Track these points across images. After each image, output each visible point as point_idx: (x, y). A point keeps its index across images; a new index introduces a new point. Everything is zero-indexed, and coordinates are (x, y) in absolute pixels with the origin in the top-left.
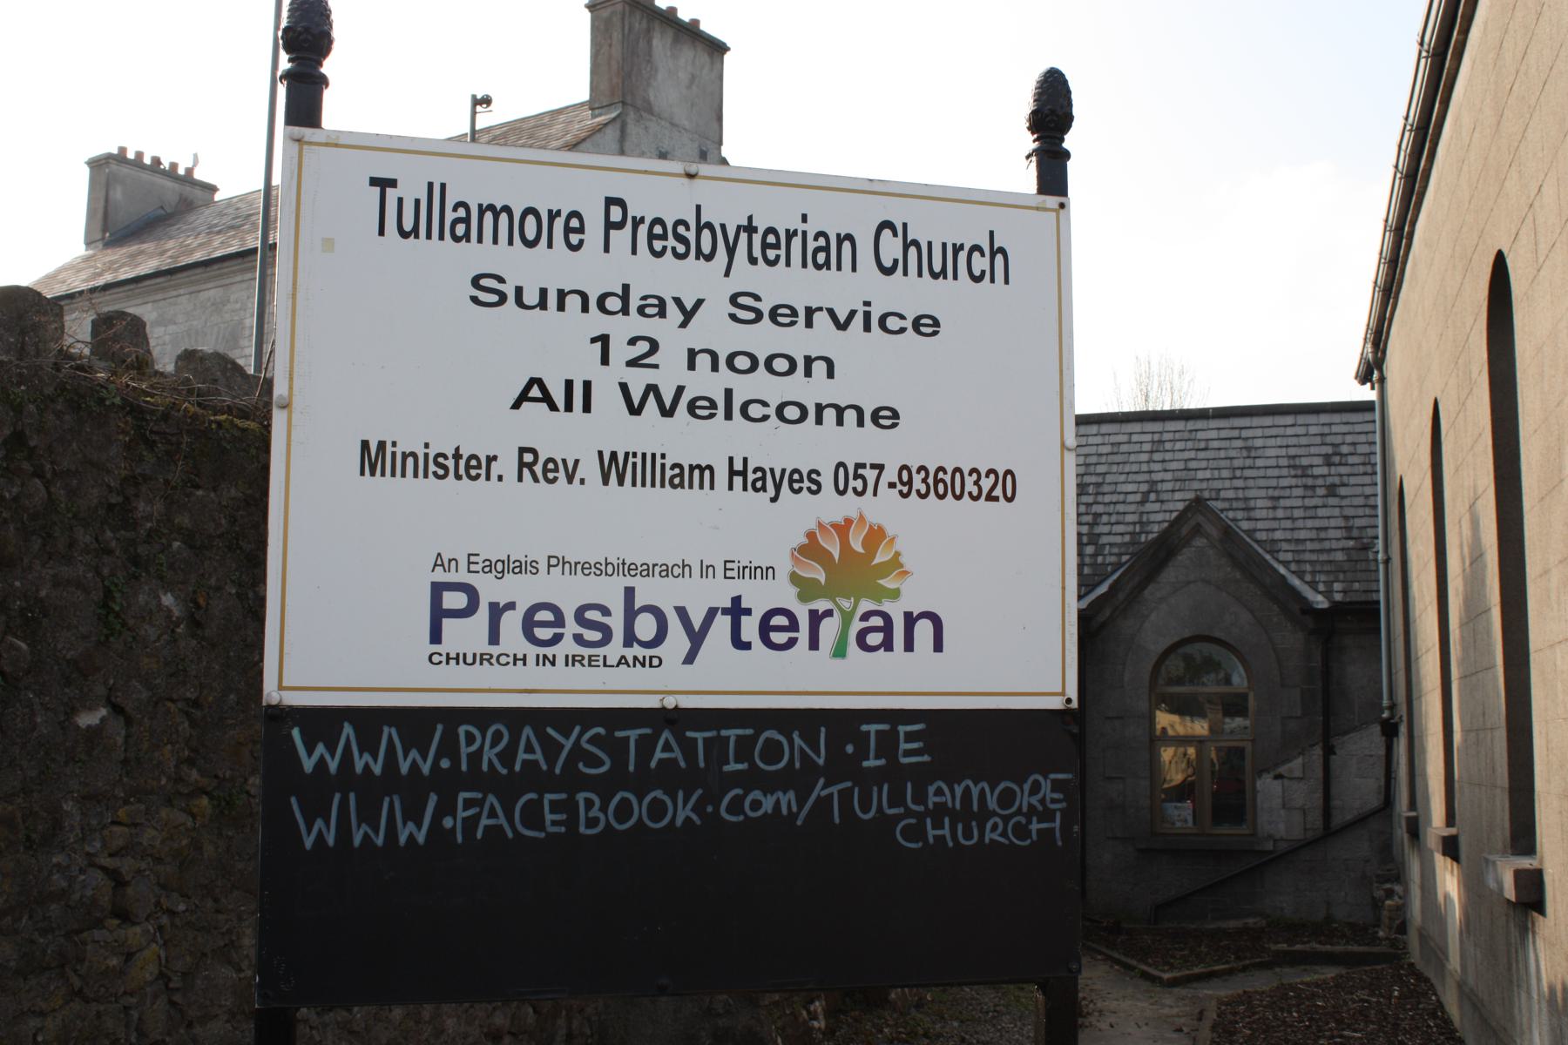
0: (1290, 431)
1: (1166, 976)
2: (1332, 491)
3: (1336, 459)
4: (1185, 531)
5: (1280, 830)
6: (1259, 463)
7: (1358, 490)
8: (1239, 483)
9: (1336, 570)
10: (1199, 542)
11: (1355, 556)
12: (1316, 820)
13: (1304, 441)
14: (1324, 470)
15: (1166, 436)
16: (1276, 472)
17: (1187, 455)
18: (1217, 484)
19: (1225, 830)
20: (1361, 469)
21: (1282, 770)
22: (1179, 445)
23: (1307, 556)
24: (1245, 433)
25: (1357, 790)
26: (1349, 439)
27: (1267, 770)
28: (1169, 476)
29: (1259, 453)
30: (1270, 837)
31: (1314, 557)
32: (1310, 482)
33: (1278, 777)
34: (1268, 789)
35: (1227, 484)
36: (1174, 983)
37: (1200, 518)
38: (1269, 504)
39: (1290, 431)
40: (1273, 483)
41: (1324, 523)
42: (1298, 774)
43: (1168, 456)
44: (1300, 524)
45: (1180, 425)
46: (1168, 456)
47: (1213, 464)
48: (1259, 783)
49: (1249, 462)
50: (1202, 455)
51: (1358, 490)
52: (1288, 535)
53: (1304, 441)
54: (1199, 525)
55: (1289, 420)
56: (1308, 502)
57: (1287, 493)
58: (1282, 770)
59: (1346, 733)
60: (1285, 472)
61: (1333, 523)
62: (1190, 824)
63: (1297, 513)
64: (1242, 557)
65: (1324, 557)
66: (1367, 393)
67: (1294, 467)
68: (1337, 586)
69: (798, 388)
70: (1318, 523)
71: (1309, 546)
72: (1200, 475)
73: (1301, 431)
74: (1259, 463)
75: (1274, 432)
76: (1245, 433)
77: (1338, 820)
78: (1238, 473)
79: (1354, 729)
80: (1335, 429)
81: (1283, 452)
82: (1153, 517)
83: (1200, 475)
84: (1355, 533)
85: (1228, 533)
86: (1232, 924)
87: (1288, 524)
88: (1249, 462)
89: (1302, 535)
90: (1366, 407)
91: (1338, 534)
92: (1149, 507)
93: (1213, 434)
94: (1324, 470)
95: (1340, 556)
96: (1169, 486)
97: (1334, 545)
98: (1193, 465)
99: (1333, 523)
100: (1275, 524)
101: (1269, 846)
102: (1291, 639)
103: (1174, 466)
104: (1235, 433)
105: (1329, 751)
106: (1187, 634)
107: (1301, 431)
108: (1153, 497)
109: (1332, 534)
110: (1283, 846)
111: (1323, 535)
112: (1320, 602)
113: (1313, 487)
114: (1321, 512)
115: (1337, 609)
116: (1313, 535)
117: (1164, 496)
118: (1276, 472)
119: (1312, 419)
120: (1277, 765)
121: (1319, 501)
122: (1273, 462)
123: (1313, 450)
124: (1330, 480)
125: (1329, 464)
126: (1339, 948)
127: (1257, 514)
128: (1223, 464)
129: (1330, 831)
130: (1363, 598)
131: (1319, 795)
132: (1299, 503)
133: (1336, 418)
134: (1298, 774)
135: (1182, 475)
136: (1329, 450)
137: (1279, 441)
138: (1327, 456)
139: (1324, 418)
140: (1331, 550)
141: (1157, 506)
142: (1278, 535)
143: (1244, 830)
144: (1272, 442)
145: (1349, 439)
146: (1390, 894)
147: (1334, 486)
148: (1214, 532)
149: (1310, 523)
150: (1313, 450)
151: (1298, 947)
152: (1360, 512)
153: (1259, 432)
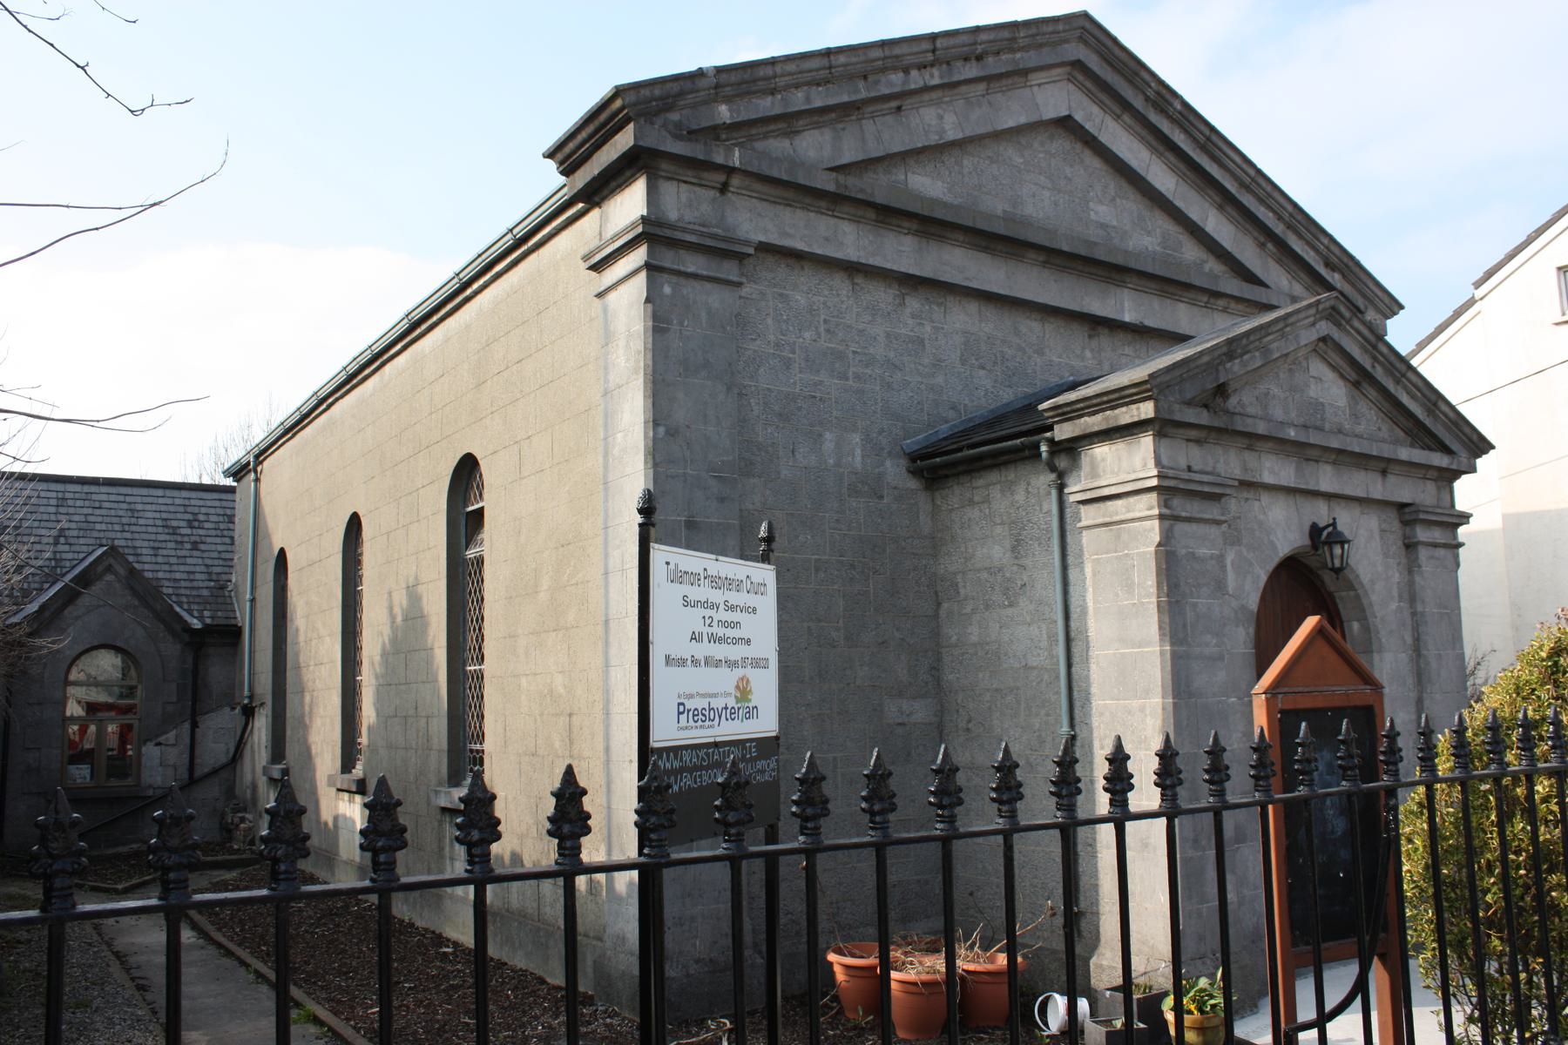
0: (161, 501)
1: (120, 887)
4: (100, 569)
6: (141, 522)
7: (213, 547)
8: (128, 535)
9: (205, 602)
10: (109, 577)
11: (215, 592)
12: (183, 773)
13: (172, 509)
14: (188, 531)
15: (68, 495)
16: (154, 530)
17: (85, 511)
18: (112, 535)
19: (114, 782)
20: (213, 533)
22: (79, 503)
23: (183, 591)
24: (128, 499)
25: (214, 750)
26: (203, 510)
28: (73, 525)
30: (150, 786)
33: (159, 744)
34: (151, 752)
35: (119, 535)
37: (112, 561)
39: (161, 501)
40: (153, 537)
41: (192, 569)
42: (172, 741)
43: (71, 510)
45: (78, 488)
46: (71, 510)
47: (108, 520)
48: (144, 749)
49: (133, 520)
50: (98, 512)
51: (213, 547)
52: (168, 575)
53: (172, 509)
55: (160, 492)
58: (161, 739)
60: (160, 530)
61: (198, 569)
63: (173, 560)
64: (143, 591)
65: (195, 593)
68: (206, 613)
69: (730, 633)
70: (187, 568)
71: (183, 584)
72: (98, 527)
74: (141, 522)
75: (150, 500)
76: (128, 499)
79: (212, 710)
80: (193, 502)
82: (64, 556)
83: (98, 527)
85: (133, 572)
87: (167, 567)
88: (133, 520)
89: (178, 576)
91: (203, 577)
92: (60, 548)
93: (104, 497)
94: (188, 531)
95: (205, 593)
96: (75, 533)
98: (91, 519)
99: (198, 569)
100: (157, 567)
101: (150, 793)
102: (172, 649)
103: (76, 518)
104: (121, 498)
105: (194, 726)
106: (96, 643)
107: (169, 501)
108: (62, 540)
109: (198, 576)
110: (159, 792)
112: (196, 624)
114: (189, 561)
115: (208, 630)
116: (185, 576)
117: (72, 541)
118: (154, 530)
119: (176, 493)
121: (187, 553)
122: (151, 522)
123: (179, 516)
124: (193, 539)
125: (192, 527)
126: (220, 858)
127: (145, 559)
128: (115, 520)
129: (193, 780)
131: (186, 756)
132: (173, 553)
133: (193, 494)
134: (172, 741)
135: (84, 525)
136: (190, 517)
137: (154, 507)
139: (185, 494)
141: (66, 548)
142: (160, 575)
143: (130, 781)
144: (149, 507)
145: (203, 510)
146: (243, 820)
147: (195, 543)
148: (122, 571)
149: (182, 568)
150: (179, 516)
153: (139, 499)
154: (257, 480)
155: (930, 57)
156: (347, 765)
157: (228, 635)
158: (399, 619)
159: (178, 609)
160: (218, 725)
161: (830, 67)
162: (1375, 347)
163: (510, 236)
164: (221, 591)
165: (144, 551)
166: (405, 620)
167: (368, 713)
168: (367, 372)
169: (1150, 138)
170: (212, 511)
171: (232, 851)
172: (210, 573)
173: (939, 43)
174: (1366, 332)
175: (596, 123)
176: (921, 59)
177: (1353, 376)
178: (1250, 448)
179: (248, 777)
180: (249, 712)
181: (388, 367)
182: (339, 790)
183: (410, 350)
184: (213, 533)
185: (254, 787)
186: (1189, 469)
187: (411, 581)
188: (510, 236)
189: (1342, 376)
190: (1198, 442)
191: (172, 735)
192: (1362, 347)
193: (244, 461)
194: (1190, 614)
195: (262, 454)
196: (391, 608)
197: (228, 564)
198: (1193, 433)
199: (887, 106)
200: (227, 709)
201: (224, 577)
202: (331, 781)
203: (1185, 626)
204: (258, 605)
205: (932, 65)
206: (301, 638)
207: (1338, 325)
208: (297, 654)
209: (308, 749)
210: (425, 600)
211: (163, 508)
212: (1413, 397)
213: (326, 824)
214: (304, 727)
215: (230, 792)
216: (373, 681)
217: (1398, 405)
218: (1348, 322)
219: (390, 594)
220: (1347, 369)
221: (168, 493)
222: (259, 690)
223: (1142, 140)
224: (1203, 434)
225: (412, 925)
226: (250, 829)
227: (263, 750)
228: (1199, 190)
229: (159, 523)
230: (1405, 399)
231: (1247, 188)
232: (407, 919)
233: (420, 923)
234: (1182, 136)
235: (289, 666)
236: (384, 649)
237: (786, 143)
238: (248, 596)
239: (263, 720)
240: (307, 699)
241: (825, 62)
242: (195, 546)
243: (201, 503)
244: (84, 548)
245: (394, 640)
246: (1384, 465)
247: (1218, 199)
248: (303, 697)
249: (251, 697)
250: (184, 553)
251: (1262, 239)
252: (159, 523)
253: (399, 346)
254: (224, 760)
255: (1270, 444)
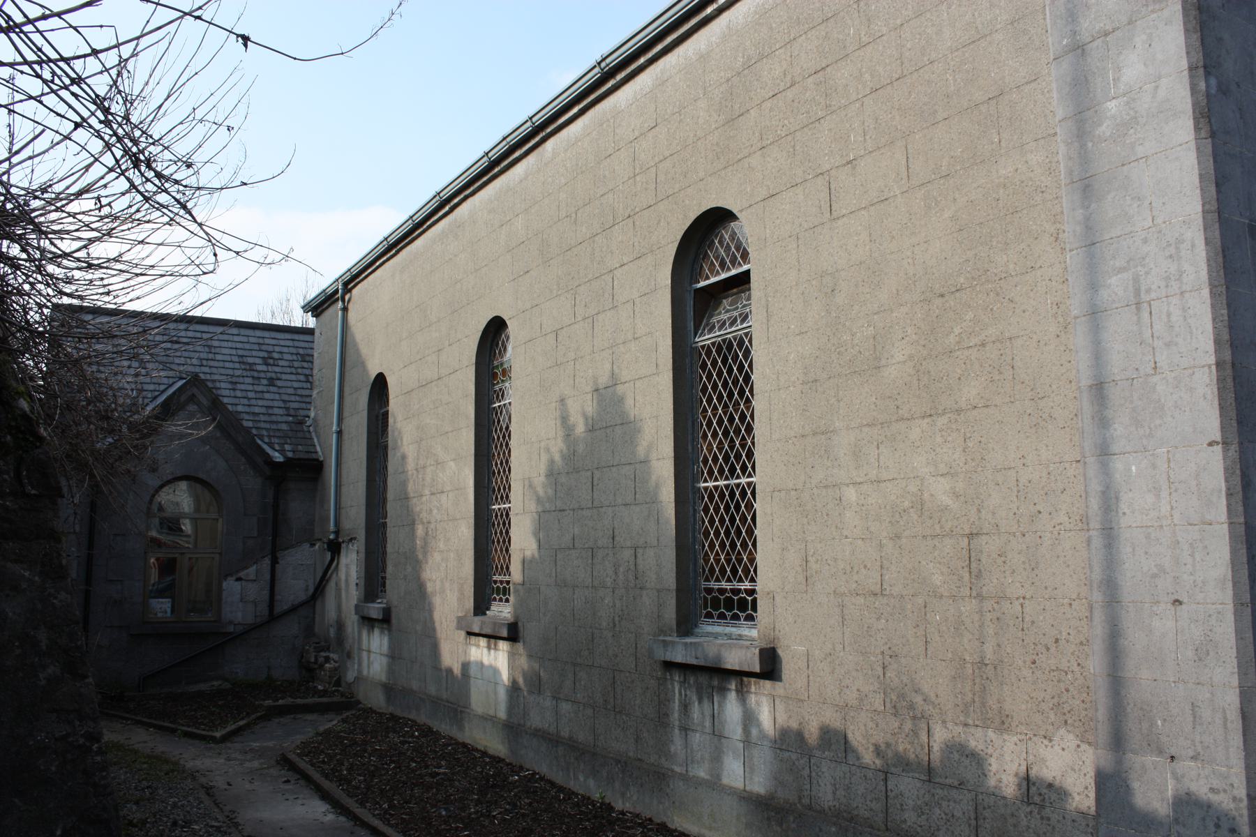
1: (218, 735)
2: (271, 382)
3: (271, 361)
4: (183, 398)
5: (239, 617)
6: (219, 357)
7: (289, 384)
10: (192, 407)
12: (263, 609)
13: (247, 346)
14: (264, 368)
16: (231, 365)
20: (289, 370)
21: (242, 574)
23: (263, 425)
25: (294, 587)
26: (277, 349)
27: (231, 575)
29: (218, 350)
30: (231, 622)
31: (268, 426)
32: (256, 374)
33: (239, 579)
34: (231, 587)
36: (225, 739)
37: (195, 390)
38: (230, 386)
39: (236, 338)
40: (230, 372)
42: (252, 577)
44: (253, 402)
48: (225, 584)
49: (211, 356)
51: (289, 384)
53: (247, 346)
54: (193, 395)
56: (256, 388)
57: (241, 380)
58: (242, 574)
59: (287, 549)
60: (237, 366)
62: (169, 614)
63: (251, 395)
65: (274, 427)
66: (311, 322)
67: (243, 363)
68: (287, 447)
71: (262, 418)
73: (245, 339)
74: (219, 357)
77: (278, 609)
78: (205, 363)
79: (292, 546)
80: (267, 341)
81: (234, 352)
82: (146, 387)
84: (292, 412)
86: (203, 687)
87: (245, 402)
88: (211, 356)
89: (257, 410)
90: (310, 332)
91: (281, 411)
95: (284, 427)
97: (280, 419)
99: (276, 404)
100: (236, 401)
101: (231, 629)
107: (245, 339)
109: (276, 411)
111: (270, 411)
112: (278, 457)
113: (259, 378)
114: (267, 396)
115: (289, 464)
116: (263, 410)
118: (231, 365)
119: (250, 332)
120: (238, 572)
121: (265, 389)
122: (228, 358)
123: (254, 353)
124: (269, 375)
125: (267, 364)
129: (273, 617)
130: (306, 456)
131: (266, 593)
132: (251, 388)
133: (266, 334)
136: (266, 355)
137: (230, 344)
138: (263, 358)
139: (258, 333)
140: (277, 422)
142: (240, 408)
144: (225, 344)
145: (277, 349)
146: (327, 659)
147: (271, 379)
148: (205, 401)
149: (260, 403)
150: (254, 353)
151: (281, 702)
152: (293, 398)
154: (345, 309)
156: (482, 600)
157: (311, 469)
158: (580, 429)
159: (259, 442)
160: (298, 566)
163: (485, 159)
164: (299, 426)
165: (223, 385)
166: (591, 429)
167: (523, 540)
168: (517, 154)
170: (285, 350)
171: (316, 693)
172: (288, 409)
179: (331, 615)
180: (335, 548)
181: (549, 144)
182: (470, 634)
183: (392, 261)
184: (289, 370)
185: (340, 626)
187: (603, 380)
188: (485, 159)
191: (251, 571)
193: (330, 291)
195: (352, 280)
196: (564, 419)
197: (307, 401)
200: (306, 546)
201: (302, 413)
202: (461, 623)
204: (345, 436)
206: (410, 465)
208: (404, 484)
209: (421, 587)
210: (629, 402)
211: (239, 345)
213: (449, 671)
214: (414, 562)
215: (309, 630)
216: (532, 506)
219: (562, 401)
221: (243, 331)
222: (347, 525)
225: (610, 808)
226: (336, 669)
227: (353, 588)
229: (236, 359)
232: (596, 796)
233: (619, 805)
235: (391, 495)
236: (552, 462)
238: (334, 428)
239: (354, 556)
240: (420, 531)
242: (271, 382)
243: (274, 342)
244: (165, 381)
245: (571, 456)
248: (413, 531)
249: (337, 533)
250: (260, 388)
252: (236, 359)
253: (575, 110)
254: (303, 597)
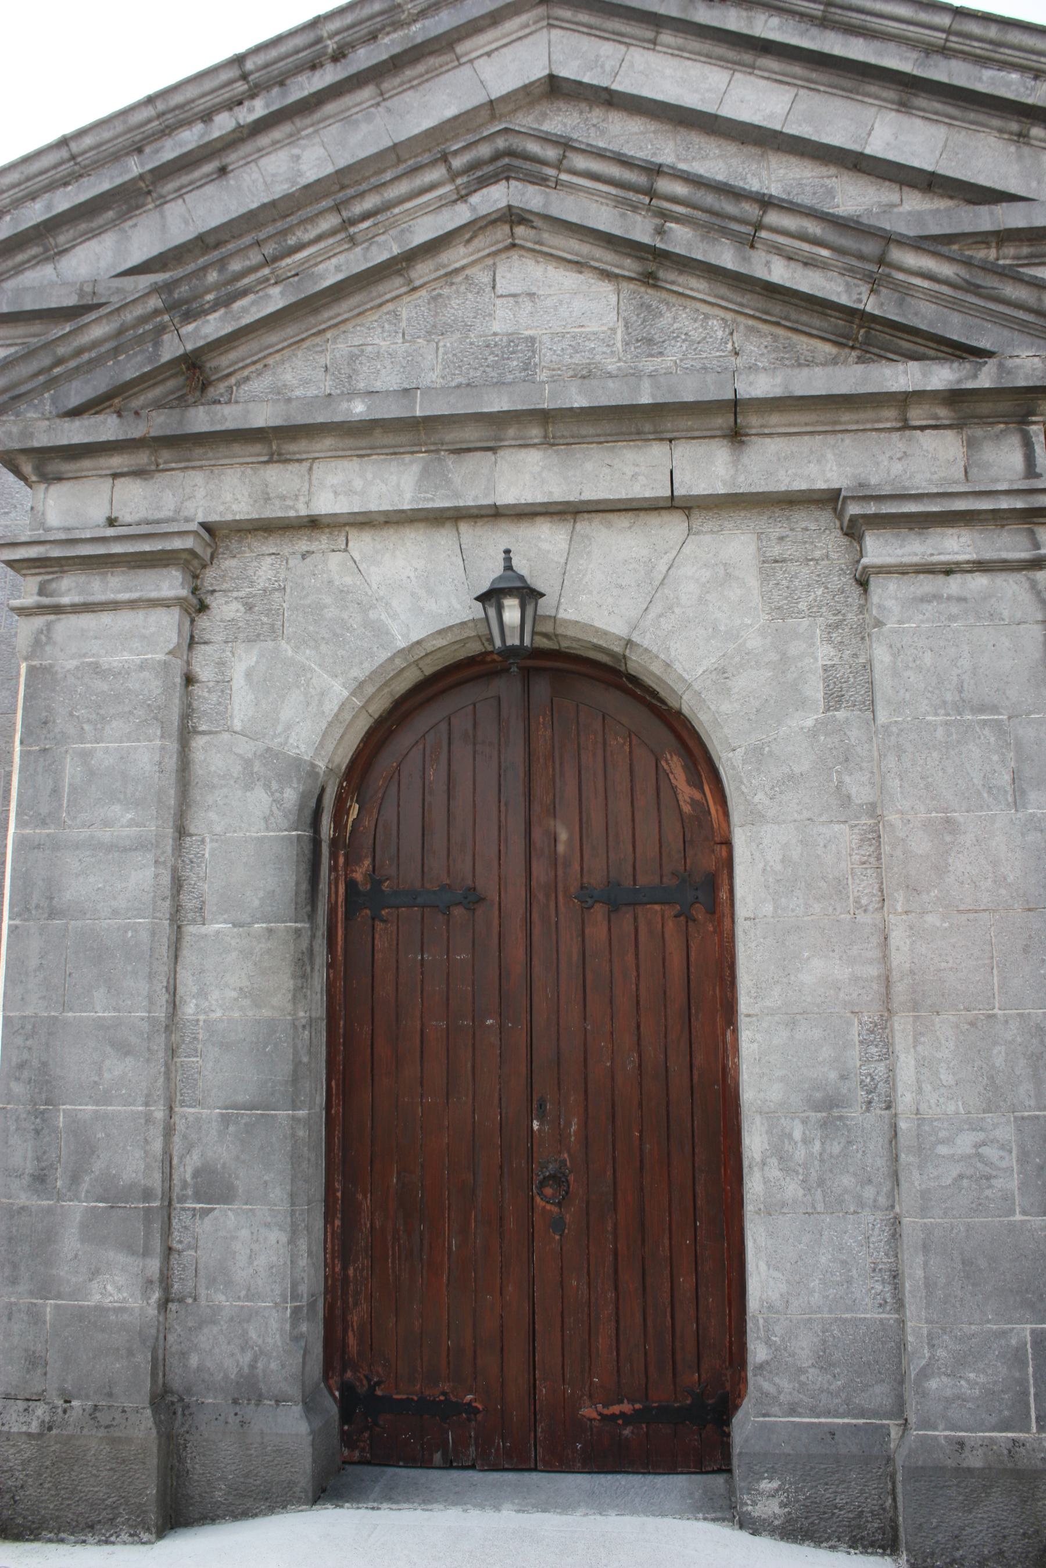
155: (241, 87)
161: (73, 157)
162: (651, 193)
169: (721, 50)
173: (249, 65)
174: (614, 171)
175: (882, 353)
176: (226, 94)
177: (629, 266)
178: (277, 458)
186: (111, 522)
189: (606, 275)
190: (139, 473)
192: (620, 202)
194: (71, 771)
198: (117, 462)
199: (197, 174)
203: (56, 791)
205: (253, 96)
207: (541, 181)
212: (810, 263)
217: (772, 290)
218: (558, 166)
220: (606, 258)
223: (710, 58)
224: (142, 458)
228: (849, 94)
230: (779, 273)
231: (944, 51)
234: (775, 21)
237: (46, 272)
241: (64, 153)
246: (732, 420)
247: (891, 95)
251: (1014, 127)
255: (328, 442)
